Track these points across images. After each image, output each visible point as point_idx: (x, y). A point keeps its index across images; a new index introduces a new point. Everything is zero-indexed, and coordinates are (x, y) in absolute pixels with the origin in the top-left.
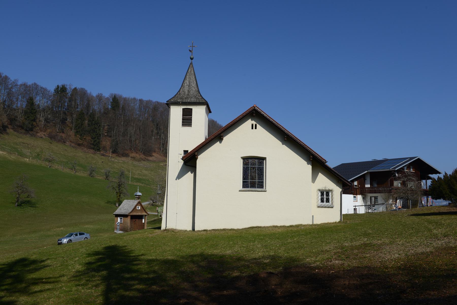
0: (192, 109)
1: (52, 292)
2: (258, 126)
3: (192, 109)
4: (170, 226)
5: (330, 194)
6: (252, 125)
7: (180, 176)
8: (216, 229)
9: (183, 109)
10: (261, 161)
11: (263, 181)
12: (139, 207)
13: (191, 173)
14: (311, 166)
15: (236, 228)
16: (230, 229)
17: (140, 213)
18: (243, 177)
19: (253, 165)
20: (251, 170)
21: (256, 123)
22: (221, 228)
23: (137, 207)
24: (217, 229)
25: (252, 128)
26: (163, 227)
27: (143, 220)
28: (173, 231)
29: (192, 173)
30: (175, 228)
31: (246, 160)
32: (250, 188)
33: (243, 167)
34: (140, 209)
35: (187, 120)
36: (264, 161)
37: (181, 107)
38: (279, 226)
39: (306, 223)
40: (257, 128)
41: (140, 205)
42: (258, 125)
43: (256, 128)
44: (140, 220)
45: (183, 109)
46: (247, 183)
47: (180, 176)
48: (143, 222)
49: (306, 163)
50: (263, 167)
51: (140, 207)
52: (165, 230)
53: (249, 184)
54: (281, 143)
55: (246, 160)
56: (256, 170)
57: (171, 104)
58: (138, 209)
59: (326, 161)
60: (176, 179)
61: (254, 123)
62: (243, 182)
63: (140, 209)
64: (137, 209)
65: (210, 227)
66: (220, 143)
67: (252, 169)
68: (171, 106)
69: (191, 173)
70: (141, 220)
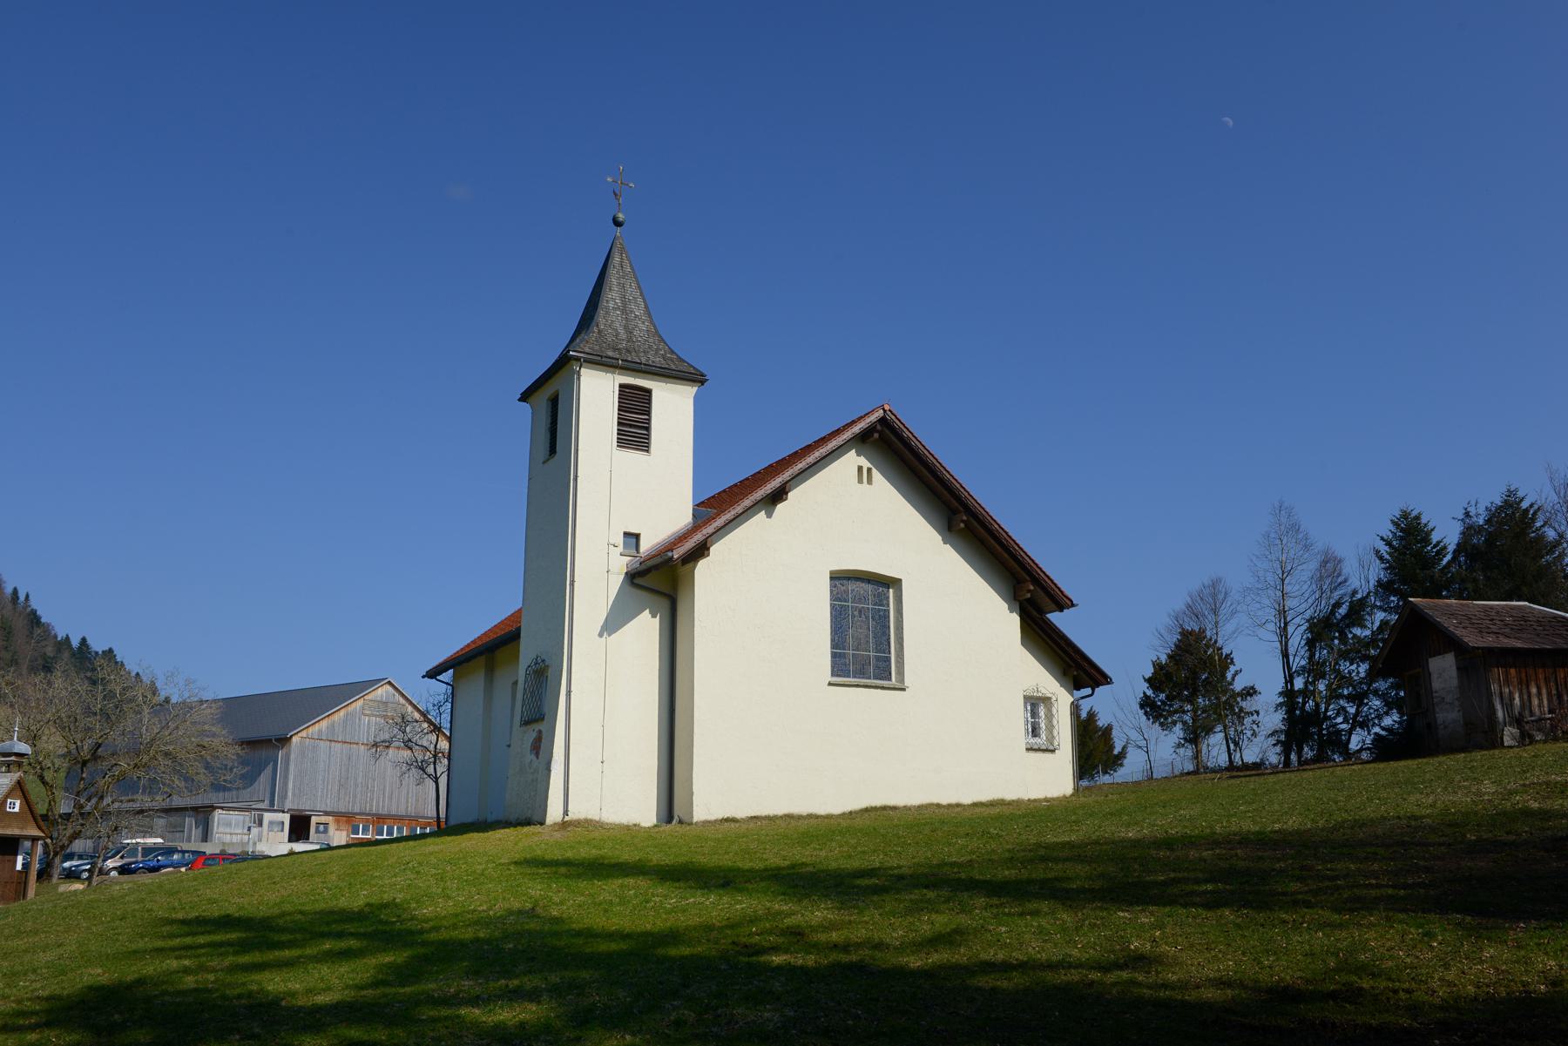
0: (649, 392)
1: (1284, 882)
2: (876, 474)
3: (649, 392)
4: (578, 811)
5: (1042, 711)
6: (860, 469)
7: (613, 624)
8: (764, 814)
9: (621, 386)
10: (881, 589)
11: (890, 657)
12: (14, 804)
13: (652, 617)
14: (1019, 618)
15: (822, 811)
16: (805, 814)
17: (18, 828)
18: (833, 640)
19: (860, 601)
20: (853, 616)
21: (870, 465)
22: (776, 813)
23: (9, 801)
24: (766, 817)
25: (860, 481)
26: (554, 813)
27: (20, 859)
28: (587, 824)
29: (654, 616)
30: (597, 818)
31: (840, 578)
32: (854, 677)
33: (833, 607)
34: (17, 809)
35: (631, 426)
36: (888, 591)
37: (617, 376)
38: (968, 805)
39: (1014, 797)
40: (873, 483)
41: (19, 793)
42: (874, 471)
43: (870, 481)
44: (7, 857)
45: (621, 386)
46: (843, 660)
47: (613, 624)
48: (19, 867)
49: (1006, 606)
50: (889, 611)
51: (18, 803)
52: (564, 825)
53: (849, 665)
54: (940, 538)
55: (840, 578)
56: (867, 618)
57: (586, 361)
58: (11, 810)
59: (1071, 601)
60: (601, 635)
61: (865, 464)
62: (834, 655)
63: (17, 809)
64: (8, 810)
65: (742, 808)
66: (769, 515)
67: (856, 613)
68: (583, 371)
69: (650, 616)
70: (11, 857)
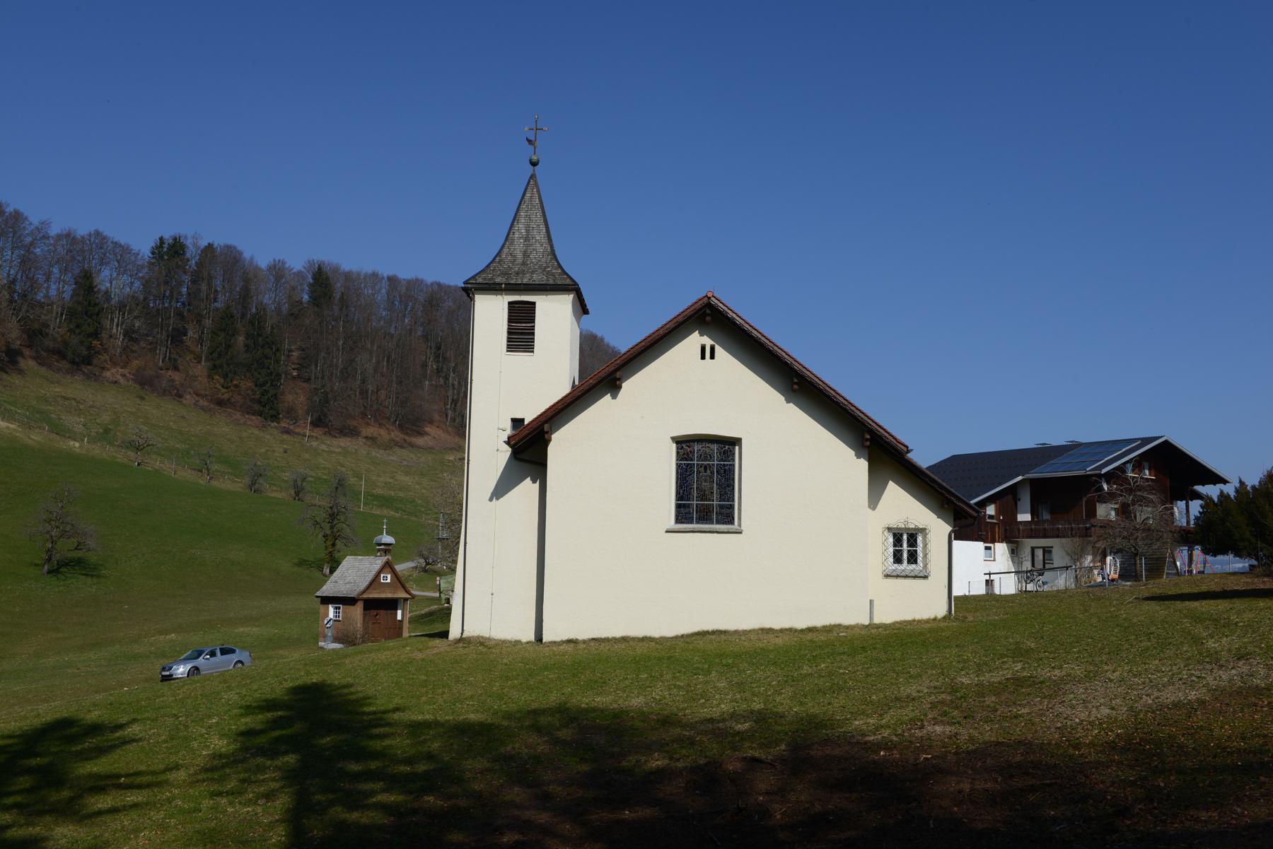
0: (534, 303)
1: (145, 814)
2: (719, 350)
3: (534, 303)
4: (473, 630)
5: (920, 539)
6: (703, 348)
7: (501, 489)
8: (603, 636)
9: (509, 303)
10: (727, 447)
11: (734, 505)
12: (387, 577)
13: (533, 483)
14: (867, 463)
15: (656, 634)
16: (641, 637)
17: (390, 593)
18: (678, 493)
19: (706, 459)
20: (699, 472)
21: (713, 343)
22: (614, 636)
23: (382, 575)
24: (605, 639)
25: (703, 357)
26: (454, 632)
27: (399, 612)
28: (481, 642)
29: (534, 482)
30: (488, 636)
31: (685, 445)
32: (697, 523)
33: (678, 466)
34: (389, 581)
35: (522, 334)
36: (734, 448)
37: (505, 297)
38: (776, 630)
39: (852, 622)
40: (716, 358)
41: (389, 569)
42: (718, 348)
43: (712, 357)
44: (389, 612)
45: (509, 303)
46: (687, 510)
47: (501, 489)
48: (399, 617)
49: (853, 453)
50: (734, 465)
51: (389, 576)
52: (461, 640)
53: (693, 513)
54: (783, 398)
55: (685, 445)
56: (712, 473)
57: (476, 289)
58: (385, 581)
59: (907, 447)
60: (491, 500)
61: (708, 341)
62: (678, 507)
63: (389, 581)
64: (382, 581)
65: (584, 631)
66: (614, 397)
67: (702, 469)
68: (476, 296)
69: (531, 482)
70: (393, 612)
